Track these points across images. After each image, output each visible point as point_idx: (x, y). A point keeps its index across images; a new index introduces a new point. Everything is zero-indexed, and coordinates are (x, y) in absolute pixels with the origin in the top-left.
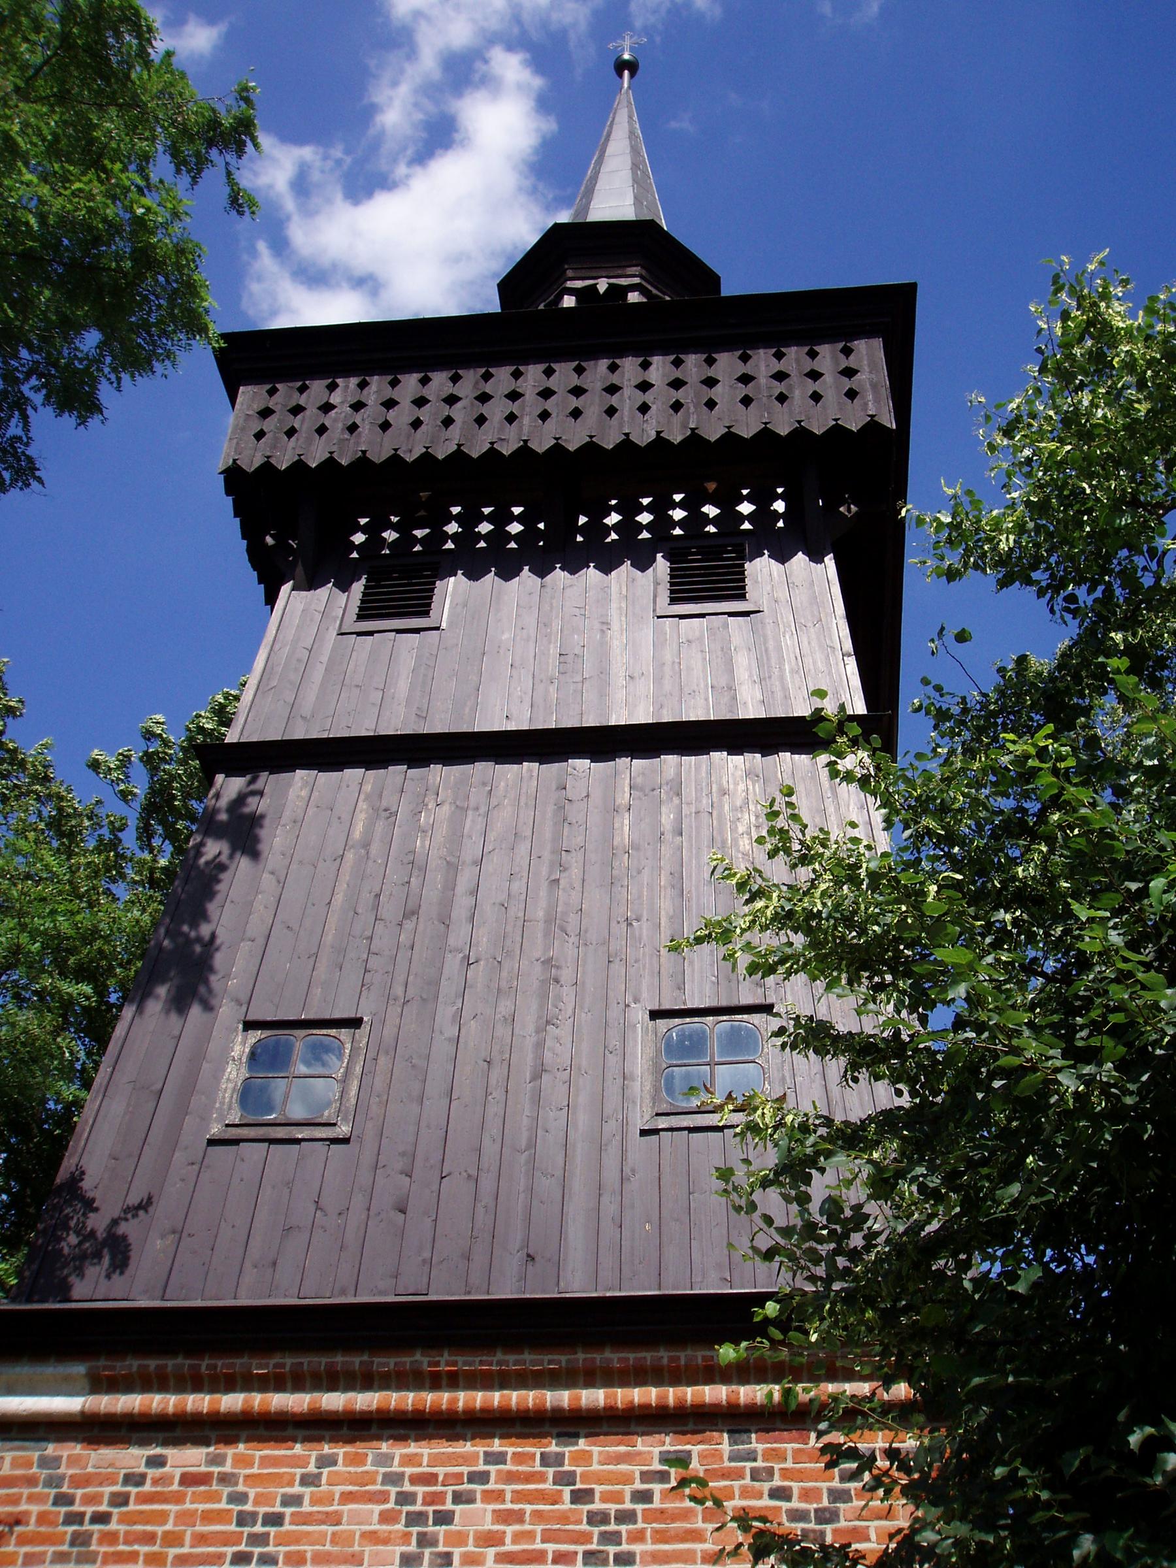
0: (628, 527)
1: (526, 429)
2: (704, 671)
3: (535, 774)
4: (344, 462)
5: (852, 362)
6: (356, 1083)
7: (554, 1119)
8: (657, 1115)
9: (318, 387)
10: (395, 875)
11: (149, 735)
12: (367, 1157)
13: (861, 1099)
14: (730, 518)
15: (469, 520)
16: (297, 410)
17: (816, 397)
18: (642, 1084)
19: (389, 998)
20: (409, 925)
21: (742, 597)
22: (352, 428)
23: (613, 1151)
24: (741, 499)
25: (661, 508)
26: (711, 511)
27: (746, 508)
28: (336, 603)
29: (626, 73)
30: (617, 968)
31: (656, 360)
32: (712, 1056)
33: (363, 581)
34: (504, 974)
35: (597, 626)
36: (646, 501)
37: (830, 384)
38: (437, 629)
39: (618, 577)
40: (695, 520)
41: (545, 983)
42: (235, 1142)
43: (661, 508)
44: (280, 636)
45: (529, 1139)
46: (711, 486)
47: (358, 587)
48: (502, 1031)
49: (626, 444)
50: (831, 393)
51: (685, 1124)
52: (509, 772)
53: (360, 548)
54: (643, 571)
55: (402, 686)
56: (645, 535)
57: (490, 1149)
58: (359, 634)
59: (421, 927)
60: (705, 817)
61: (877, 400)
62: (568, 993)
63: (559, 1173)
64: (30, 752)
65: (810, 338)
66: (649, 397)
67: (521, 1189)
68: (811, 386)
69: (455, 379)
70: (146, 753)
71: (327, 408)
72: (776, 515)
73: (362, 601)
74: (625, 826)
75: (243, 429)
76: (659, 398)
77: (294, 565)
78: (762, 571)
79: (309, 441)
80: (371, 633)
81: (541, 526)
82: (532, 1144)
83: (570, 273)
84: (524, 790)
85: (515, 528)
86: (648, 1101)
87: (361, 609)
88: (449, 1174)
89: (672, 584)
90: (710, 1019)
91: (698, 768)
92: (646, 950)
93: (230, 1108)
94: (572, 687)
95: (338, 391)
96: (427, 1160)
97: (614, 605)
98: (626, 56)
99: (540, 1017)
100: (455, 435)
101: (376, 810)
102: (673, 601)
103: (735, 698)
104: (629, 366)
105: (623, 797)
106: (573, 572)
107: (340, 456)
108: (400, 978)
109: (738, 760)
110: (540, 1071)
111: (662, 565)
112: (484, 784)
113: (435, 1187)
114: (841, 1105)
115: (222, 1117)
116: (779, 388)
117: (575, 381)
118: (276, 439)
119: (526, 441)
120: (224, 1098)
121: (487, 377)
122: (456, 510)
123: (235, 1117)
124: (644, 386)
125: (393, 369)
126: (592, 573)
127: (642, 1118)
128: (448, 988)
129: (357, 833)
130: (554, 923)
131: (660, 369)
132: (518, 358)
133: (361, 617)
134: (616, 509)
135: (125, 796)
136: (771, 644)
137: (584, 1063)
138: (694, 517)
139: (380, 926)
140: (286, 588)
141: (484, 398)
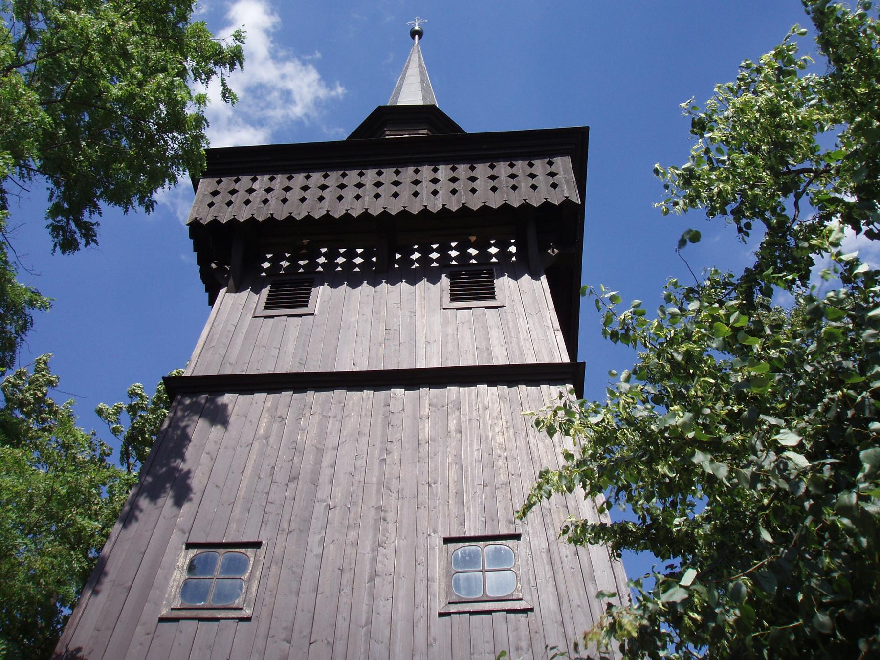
0: (425, 260)
1: (366, 203)
2: (472, 338)
3: (371, 397)
4: (260, 219)
5: (553, 169)
6: (256, 582)
7: (383, 606)
8: (450, 603)
9: (246, 180)
10: (284, 454)
11: (133, 394)
12: (263, 630)
13: (579, 594)
14: (484, 256)
15: (332, 255)
16: (233, 192)
17: (534, 187)
18: (438, 585)
19: (279, 530)
20: (292, 485)
21: (493, 298)
22: (266, 202)
23: (422, 625)
24: (490, 246)
25: (444, 250)
26: (473, 252)
27: (493, 250)
28: (252, 301)
29: (417, 36)
30: (423, 512)
31: (442, 168)
32: (484, 566)
33: (269, 288)
34: (352, 515)
35: (408, 314)
36: (435, 246)
37: (542, 180)
38: (312, 314)
39: (420, 286)
40: (464, 257)
41: (377, 521)
42: (176, 620)
43: (444, 250)
44: (218, 318)
45: (367, 618)
46: (473, 238)
47: (265, 292)
48: (350, 551)
49: (425, 212)
50: (542, 184)
51: (467, 609)
52: (356, 395)
53: (266, 270)
54: (434, 284)
55: (291, 347)
56: (435, 264)
57: (342, 625)
58: (265, 317)
59: (300, 487)
60: (475, 423)
61: (569, 189)
62: (391, 527)
63: (386, 641)
64: (61, 407)
65: (530, 156)
66: (437, 187)
67: (362, 651)
68: (531, 182)
69: (326, 176)
70: (130, 406)
71: (251, 191)
72: (511, 255)
73: (268, 299)
74: (426, 430)
75: (202, 201)
76: (444, 187)
77: (228, 279)
78: (504, 284)
79: (240, 208)
80: (272, 317)
81: (374, 259)
82: (369, 622)
83: (387, 132)
84: (364, 406)
85: (358, 260)
86: (443, 594)
87: (267, 303)
88: (315, 642)
89: (451, 291)
90: (481, 543)
91: (470, 394)
92: (441, 501)
93: (175, 598)
94: (393, 347)
95: (258, 182)
96: (301, 632)
97: (417, 302)
98: (417, 28)
99: (374, 542)
100: (325, 204)
101: (273, 417)
102: (452, 300)
103: (491, 354)
104: (426, 171)
105: (425, 411)
106: (393, 284)
107: (258, 216)
108: (287, 517)
109: (494, 389)
110: (374, 576)
111: (445, 281)
112: (340, 403)
113: (306, 650)
114: (566, 598)
115: (169, 603)
116: (512, 182)
117: (395, 178)
118: (221, 207)
119: (366, 210)
120: (171, 591)
121: (344, 175)
122: (324, 250)
123: (177, 603)
124: (435, 181)
125: (290, 170)
126: (404, 285)
127: (439, 606)
128: (316, 524)
129: (261, 431)
130: (383, 485)
131: (444, 172)
132: (362, 165)
133: (266, 308)
134: (418, 250)
135: (115, 431)
136: (511, 325)
137: (402, 571)
138: (466, 252)
139: (274, 486)
140: (222, 292)
141: (342, 186)
